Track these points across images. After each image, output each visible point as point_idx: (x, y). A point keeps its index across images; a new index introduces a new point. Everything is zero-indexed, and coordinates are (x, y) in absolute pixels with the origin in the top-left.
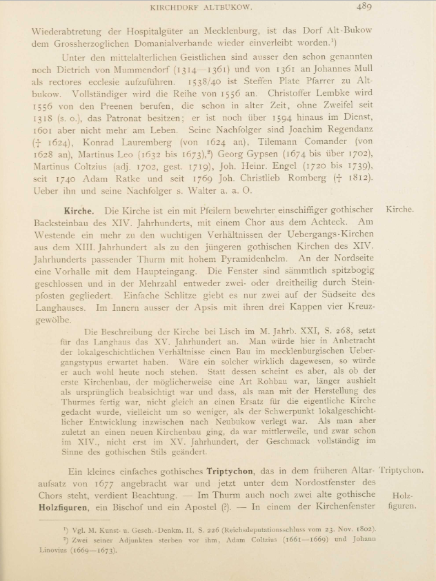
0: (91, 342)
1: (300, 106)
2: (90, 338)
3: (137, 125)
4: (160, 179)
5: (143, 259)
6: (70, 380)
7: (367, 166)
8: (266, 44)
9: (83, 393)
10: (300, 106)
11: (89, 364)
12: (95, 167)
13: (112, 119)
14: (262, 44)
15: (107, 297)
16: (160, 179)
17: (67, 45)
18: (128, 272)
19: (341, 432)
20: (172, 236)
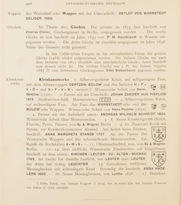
0: (48, 58)
1: (62, 120)
2: (48, 56)
3: (107, 82)
4: (45, 90)
5: (48, 27)
6: (118, 138)
7: (28, 139)
8: (77, 90)
9: (150, 66)
10: (62, 120)
11: (158, 66)
12: (82, 90)
13: (142, 66)
14: (48, 62)
15: (86, 90)
16: (45, 90)
17: (159, 54)
18: (42, 67)
19: (116, 67)
20: (105, 14)
